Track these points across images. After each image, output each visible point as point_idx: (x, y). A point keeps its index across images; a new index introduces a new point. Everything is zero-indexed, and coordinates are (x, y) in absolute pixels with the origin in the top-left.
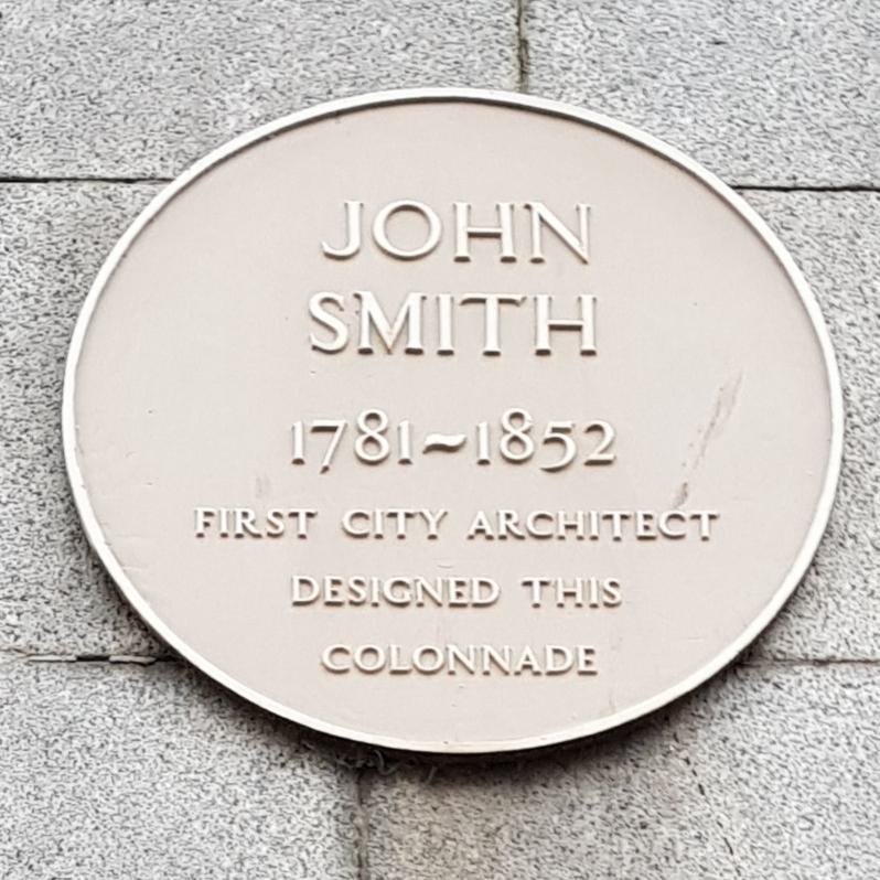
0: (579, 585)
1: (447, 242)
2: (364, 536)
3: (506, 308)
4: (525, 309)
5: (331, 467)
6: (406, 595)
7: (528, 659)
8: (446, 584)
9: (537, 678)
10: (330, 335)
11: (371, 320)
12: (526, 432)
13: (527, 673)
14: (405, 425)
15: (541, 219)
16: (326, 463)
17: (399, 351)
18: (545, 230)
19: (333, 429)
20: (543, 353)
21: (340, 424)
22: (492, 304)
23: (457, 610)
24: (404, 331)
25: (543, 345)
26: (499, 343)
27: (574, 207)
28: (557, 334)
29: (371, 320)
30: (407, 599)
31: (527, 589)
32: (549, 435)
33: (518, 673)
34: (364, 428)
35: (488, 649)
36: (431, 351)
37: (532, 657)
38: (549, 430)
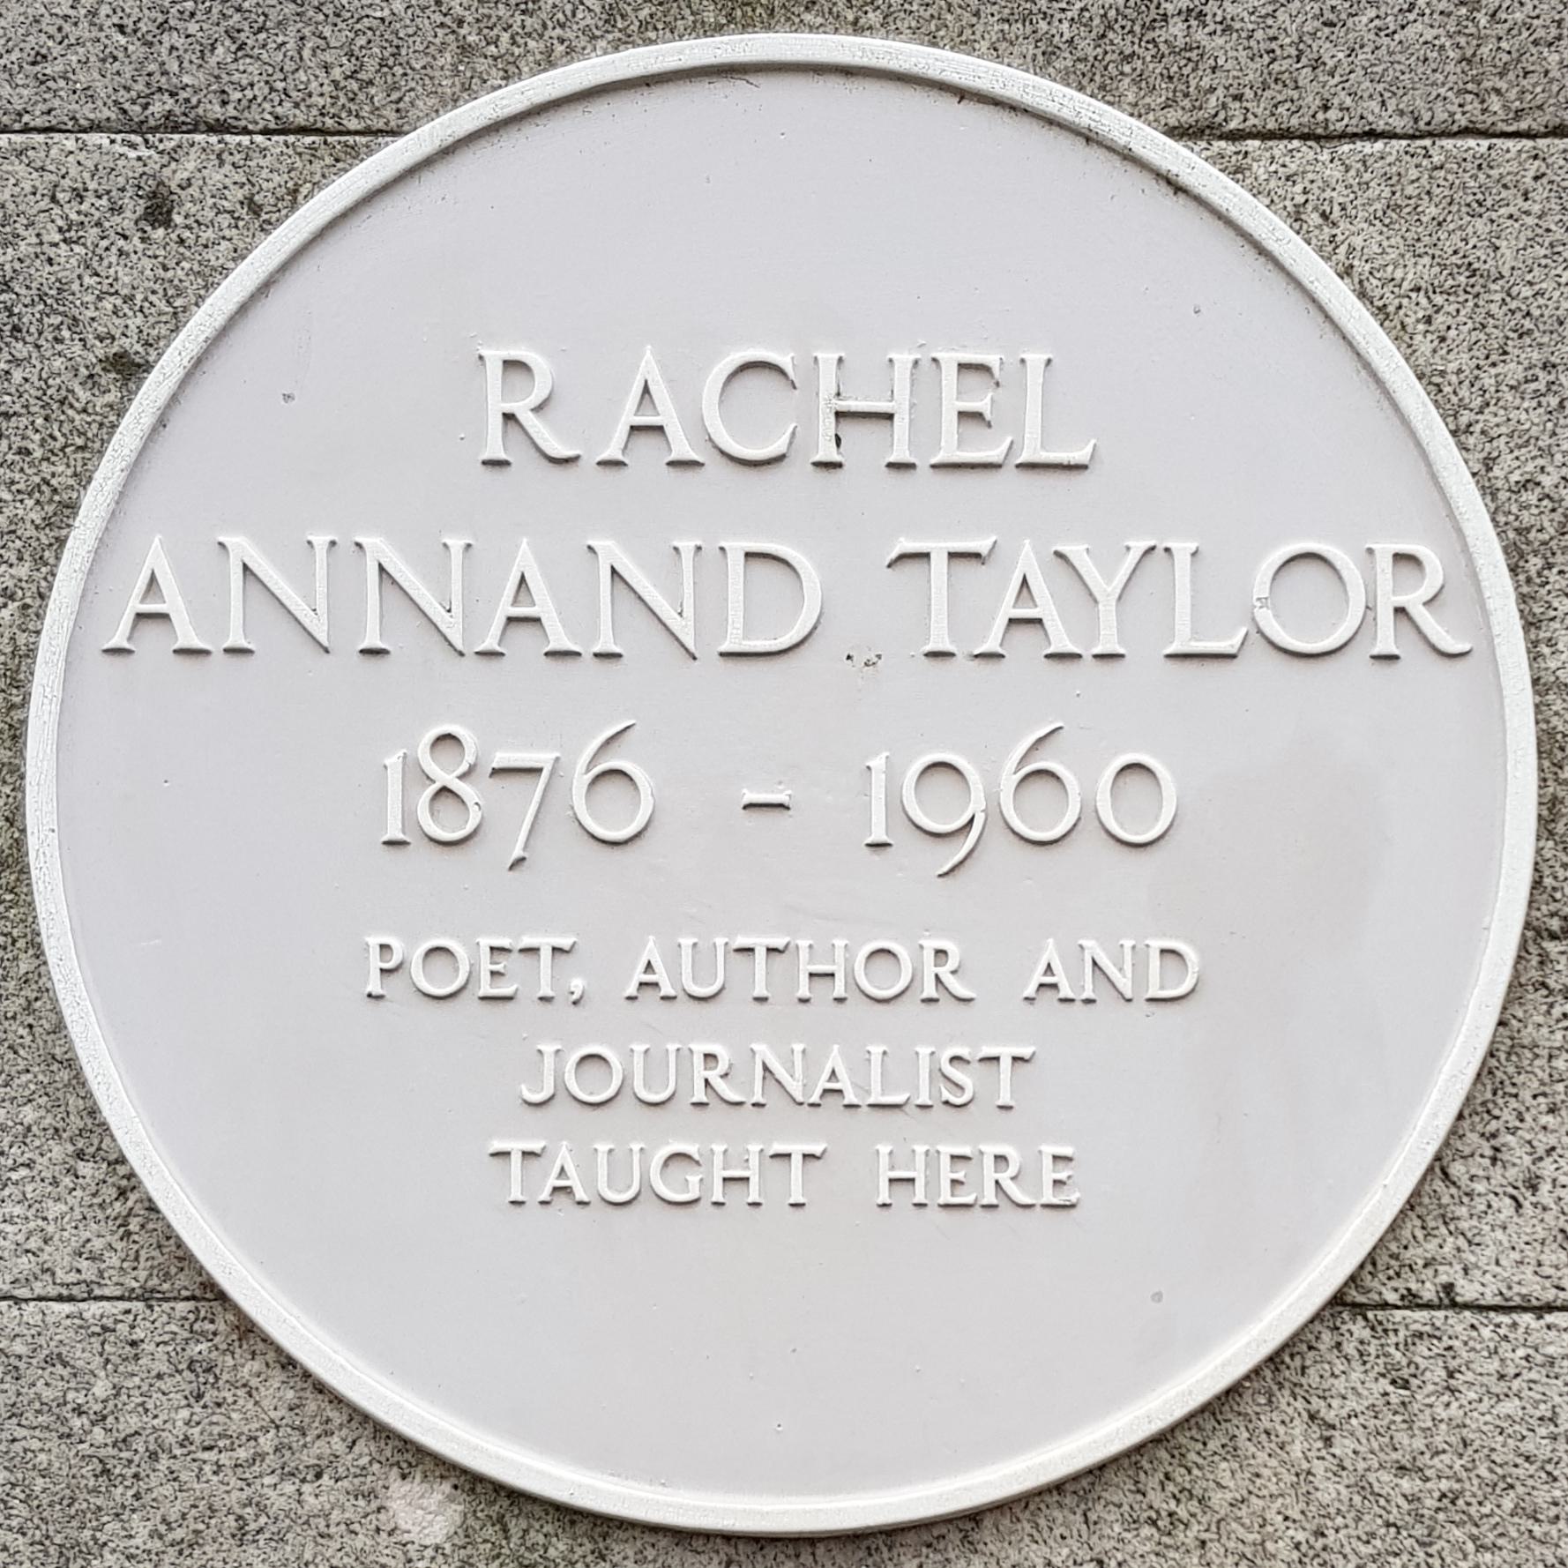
0: (754, 1161)
2: (740, 1104)
12: (461, 777)
16: (518, 852)
19: (537, 771)
23: (957, 1215)
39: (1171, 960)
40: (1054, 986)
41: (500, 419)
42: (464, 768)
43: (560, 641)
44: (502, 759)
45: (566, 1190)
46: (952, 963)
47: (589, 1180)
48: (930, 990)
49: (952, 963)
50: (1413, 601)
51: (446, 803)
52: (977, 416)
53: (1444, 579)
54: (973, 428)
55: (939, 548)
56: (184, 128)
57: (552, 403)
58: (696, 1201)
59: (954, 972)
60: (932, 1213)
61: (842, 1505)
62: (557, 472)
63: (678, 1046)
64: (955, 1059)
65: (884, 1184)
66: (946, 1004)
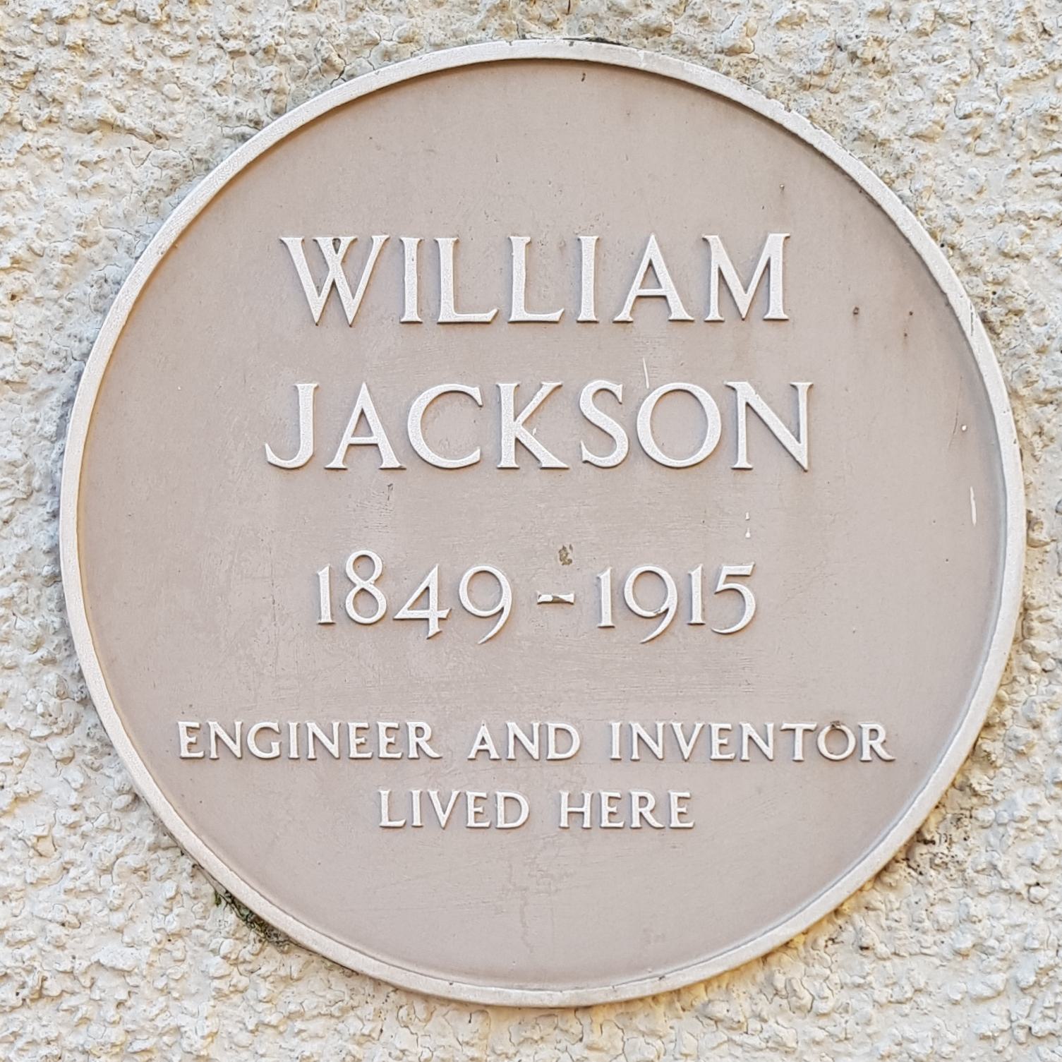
7: (483, 741)
8: (596, 799)
32: (721, 587)
38: (723, 577)
39: (561, 735)
42: (375, 577)
43: (679, 312)
55: (800, 727)
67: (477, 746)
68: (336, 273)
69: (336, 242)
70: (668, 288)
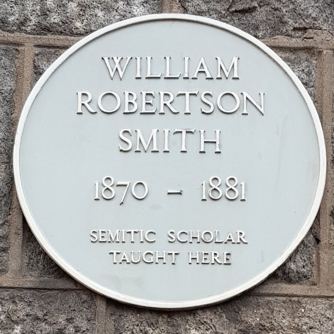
0: (164, 255)
1: (241, 108)
2: (221, 264)
3: (189, 135)
4: (196, 135)
5: (124, 202)
6: (151, 259)
9: (233, 245)
10: (125, 145)
11: (140, 140)
12: (235, 187)
13: (230, 242)
14: (243, 184)
15: (247, 98)
16: (122, 201)
17: (149, 152)
18: (249, 103)
19: (126, 185)
20: (190, 264)
21: (127, 183)
22: (184, 133)
23: (205, 265)
24: (152, 142)
25: (190, 262)
26: (169, 147)
27: (76, 93)
28: (207, 144)
29: (140, 140)
30: (152, 261)
31: (111, 255)
33: (120, 263)
34: (212, 184)
35: (246, 95)
36: (161, 152)
37: (231, 236)
40: (231, 240)
41: (81, 104)
43: (209, 76)
44: (119, 183)
45: (126, 260)
46: (243, 235)
47: (130, 258)
48: (239, 241)
49: (243, 235)
50: (86, 103)
51: (108, 192)
52: (150, 104)
53: (92, 97)
54: (149, 106)
56: (11, 32)
57: (92, 102)
58: (152, 262)
59: (244, 237)
60: (200, 265)
61: (148, 302)
62: (93, 115)
63: (199, 252)
64: (94, 232)
65: (190, 259)
66: (242, 243)
67: (228, 238)
68: (117, 66)
69: (117, 58)
70: (205, 70)
